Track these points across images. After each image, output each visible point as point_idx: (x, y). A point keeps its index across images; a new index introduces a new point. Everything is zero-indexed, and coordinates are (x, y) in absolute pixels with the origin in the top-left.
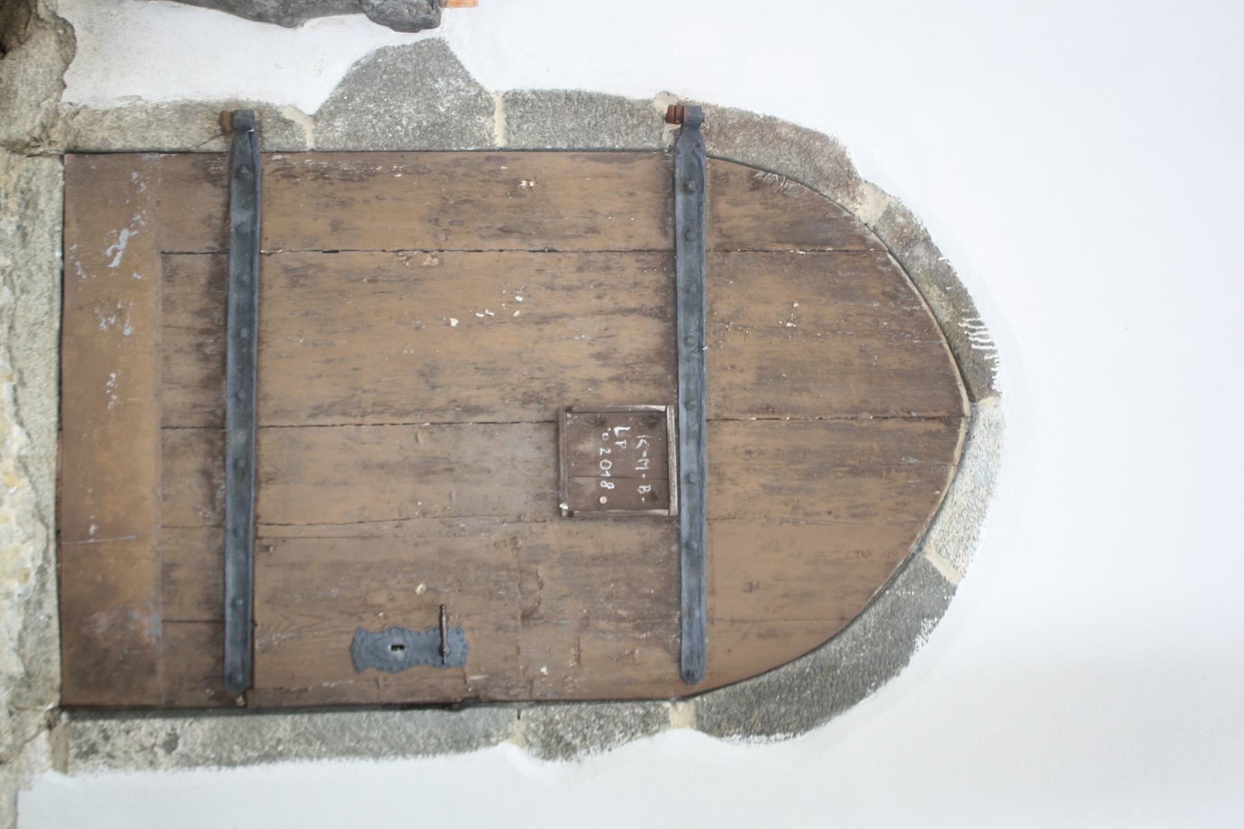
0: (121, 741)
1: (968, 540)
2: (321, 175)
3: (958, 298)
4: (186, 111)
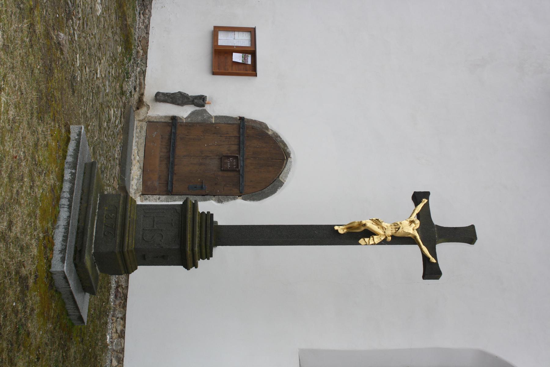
0: (151, 198)
1: (286, 177)
2: (186, 125)
3: (285, 145)
4: (166, 117)
